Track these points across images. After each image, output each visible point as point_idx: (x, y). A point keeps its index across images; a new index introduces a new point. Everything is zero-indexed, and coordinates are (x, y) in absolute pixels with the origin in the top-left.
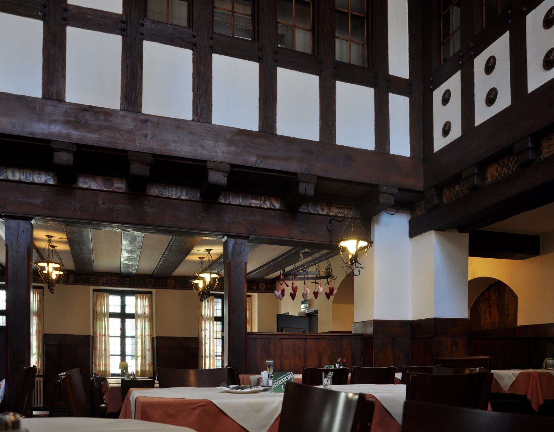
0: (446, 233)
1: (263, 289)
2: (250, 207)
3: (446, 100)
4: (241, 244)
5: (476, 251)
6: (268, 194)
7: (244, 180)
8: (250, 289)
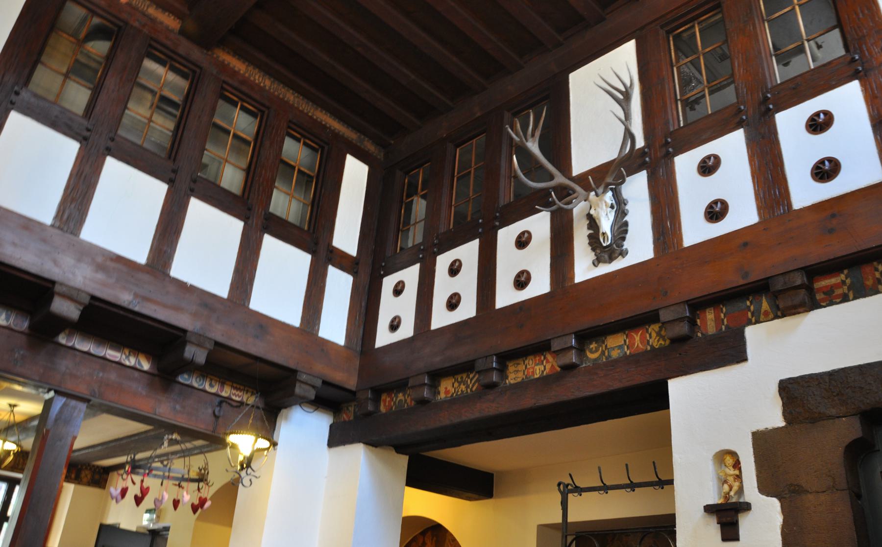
0: (378, 450)
1: (85, 480)
2: (104, 358)
3: (398, 290)
4: (75, 408)
5: (415, 480)
6: (136, 348)
7: (105, 320)
8: (68, 479)
